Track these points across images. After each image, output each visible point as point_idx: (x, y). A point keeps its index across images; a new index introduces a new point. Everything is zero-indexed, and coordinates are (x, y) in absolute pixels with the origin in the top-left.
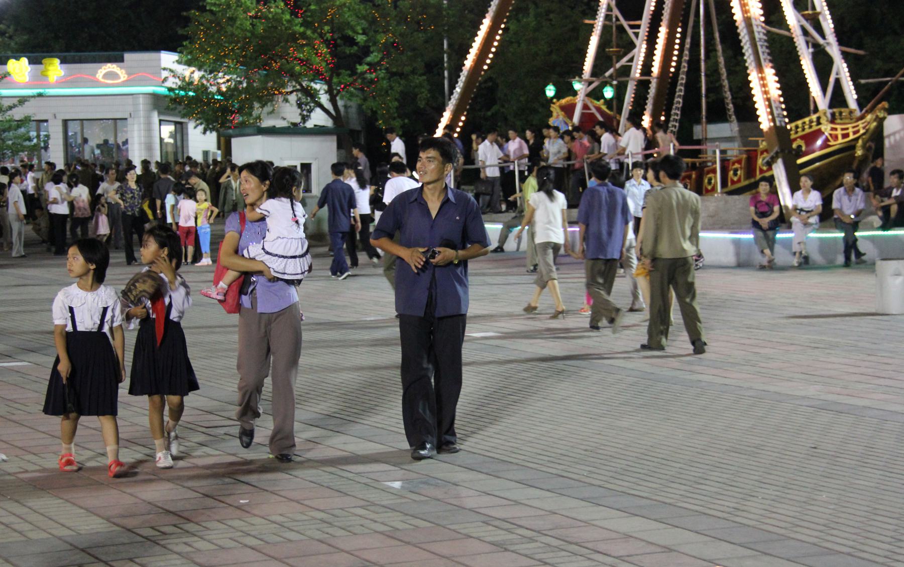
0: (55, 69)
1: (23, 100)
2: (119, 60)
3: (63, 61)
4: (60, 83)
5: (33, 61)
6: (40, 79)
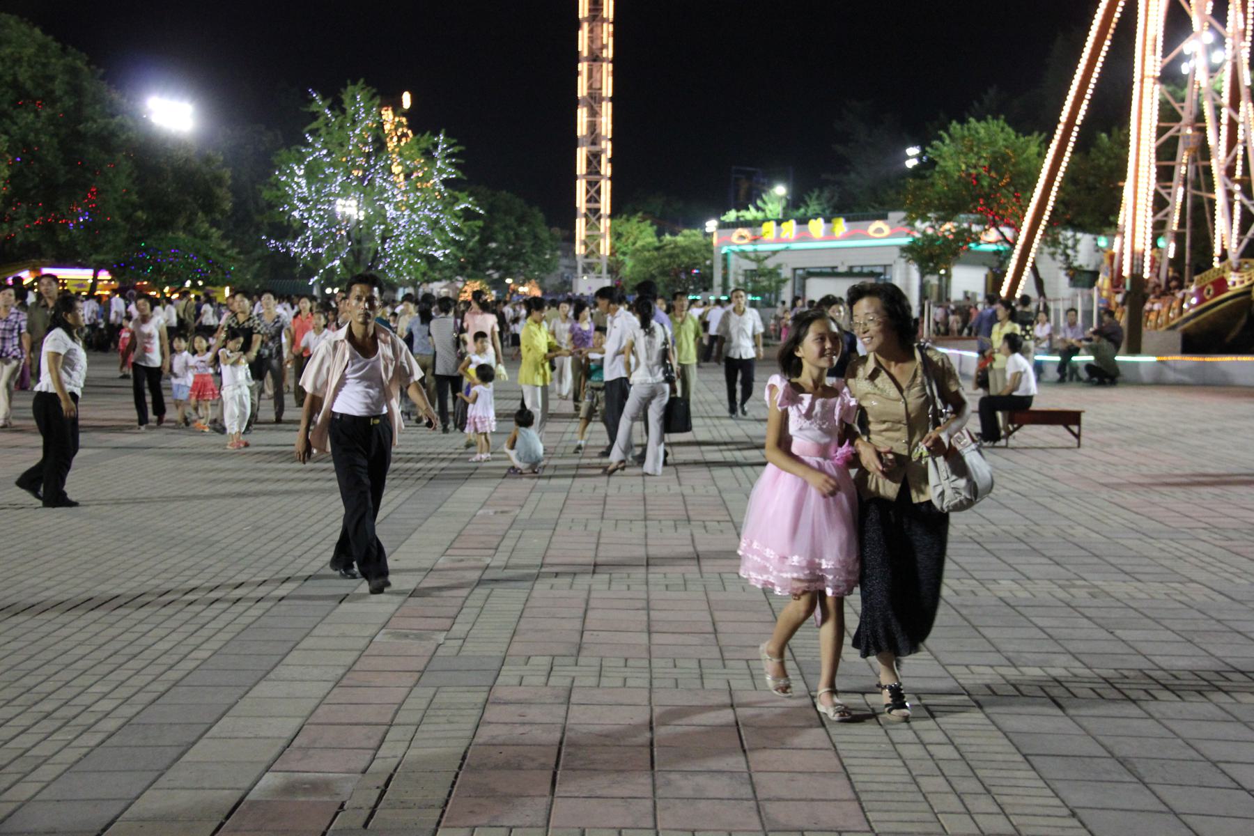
0: (841, 226)
1: (775, 253)
2: (883, 217)
3: (848, 220)
4: (846, 237)
5: (828, 220)
6: (830, 236)
